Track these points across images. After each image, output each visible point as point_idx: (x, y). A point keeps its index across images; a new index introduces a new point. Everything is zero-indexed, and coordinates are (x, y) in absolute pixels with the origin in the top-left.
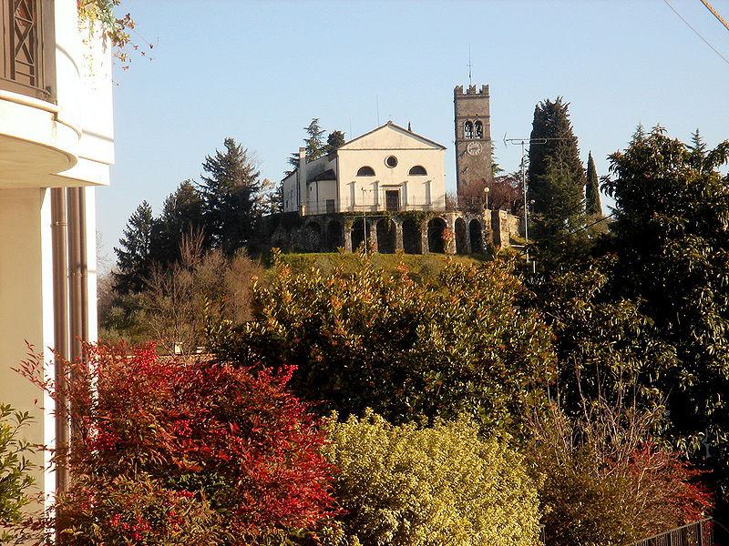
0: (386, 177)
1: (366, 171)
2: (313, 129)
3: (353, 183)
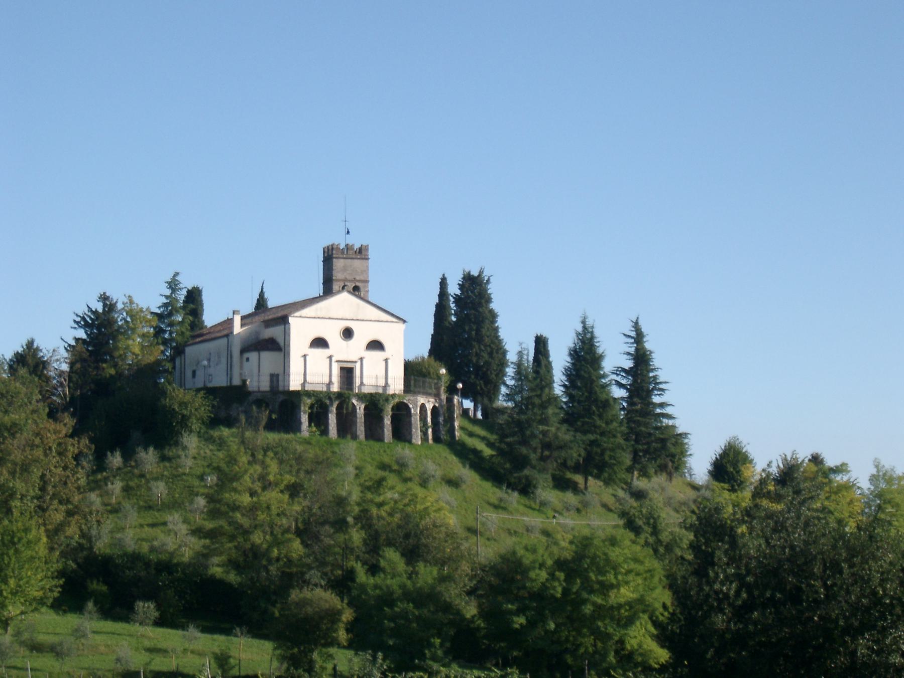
0: (341, 350)
1: (320, 343)
2: (173, 285)
3: (305, 356)
